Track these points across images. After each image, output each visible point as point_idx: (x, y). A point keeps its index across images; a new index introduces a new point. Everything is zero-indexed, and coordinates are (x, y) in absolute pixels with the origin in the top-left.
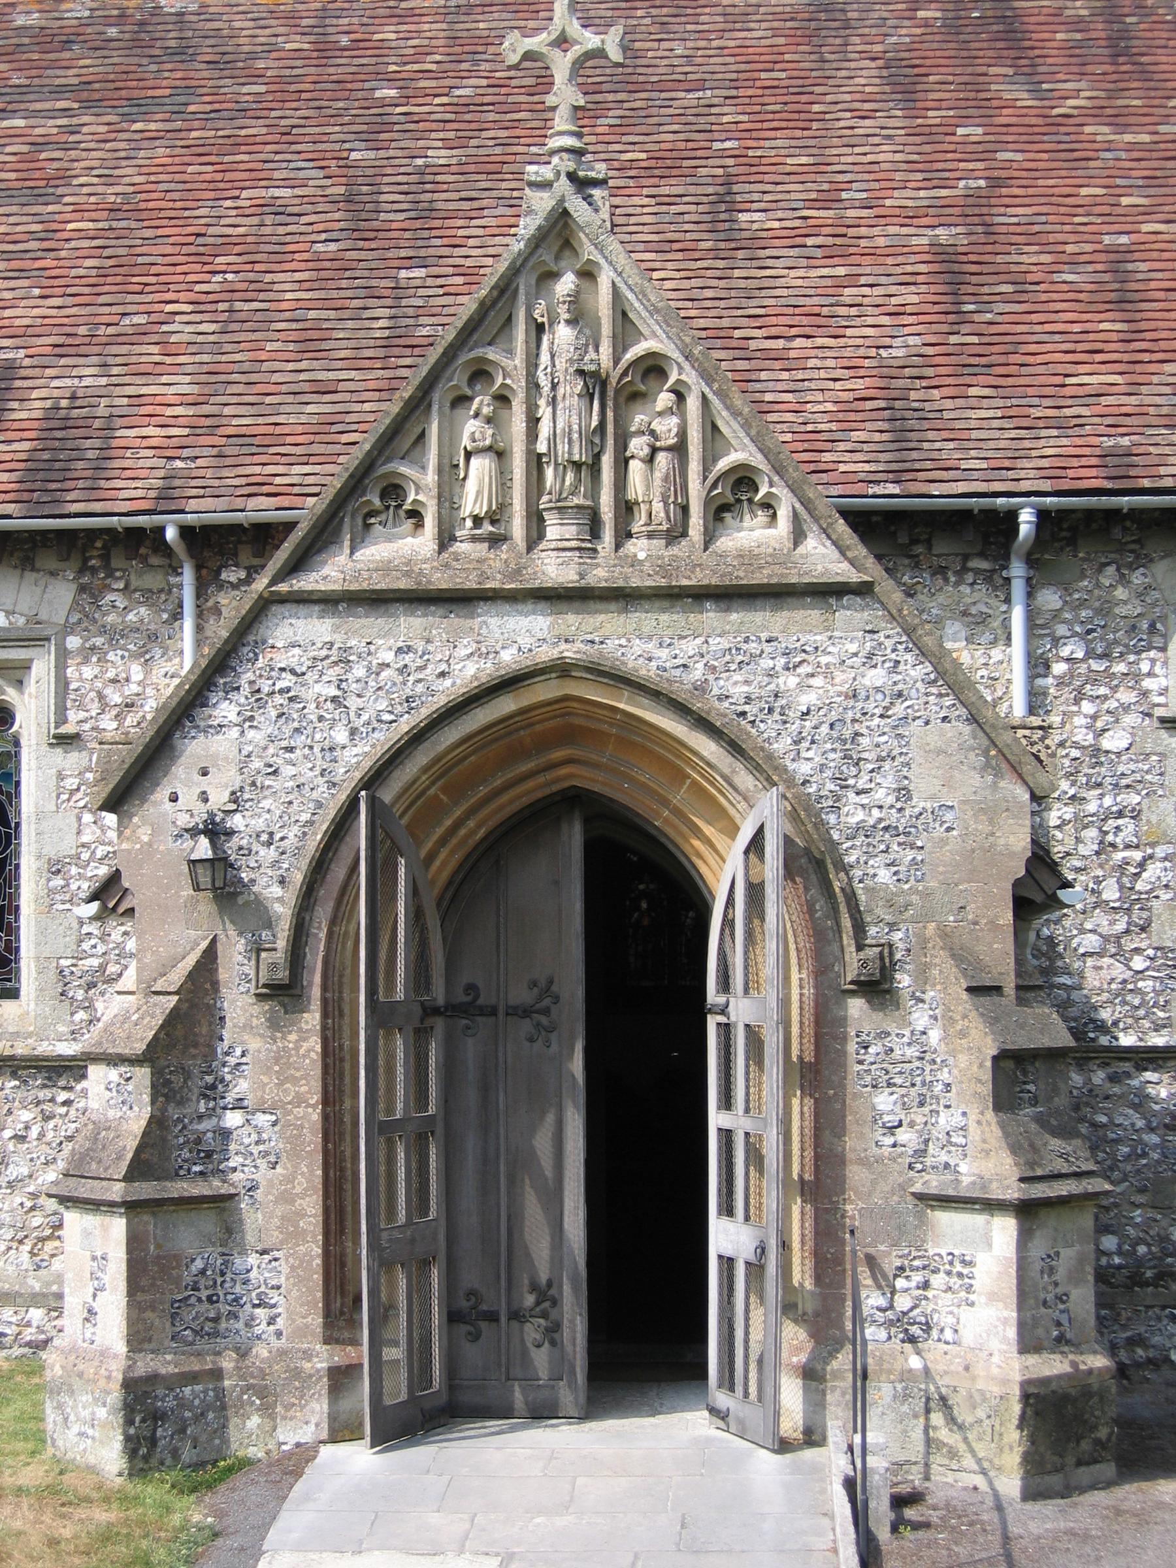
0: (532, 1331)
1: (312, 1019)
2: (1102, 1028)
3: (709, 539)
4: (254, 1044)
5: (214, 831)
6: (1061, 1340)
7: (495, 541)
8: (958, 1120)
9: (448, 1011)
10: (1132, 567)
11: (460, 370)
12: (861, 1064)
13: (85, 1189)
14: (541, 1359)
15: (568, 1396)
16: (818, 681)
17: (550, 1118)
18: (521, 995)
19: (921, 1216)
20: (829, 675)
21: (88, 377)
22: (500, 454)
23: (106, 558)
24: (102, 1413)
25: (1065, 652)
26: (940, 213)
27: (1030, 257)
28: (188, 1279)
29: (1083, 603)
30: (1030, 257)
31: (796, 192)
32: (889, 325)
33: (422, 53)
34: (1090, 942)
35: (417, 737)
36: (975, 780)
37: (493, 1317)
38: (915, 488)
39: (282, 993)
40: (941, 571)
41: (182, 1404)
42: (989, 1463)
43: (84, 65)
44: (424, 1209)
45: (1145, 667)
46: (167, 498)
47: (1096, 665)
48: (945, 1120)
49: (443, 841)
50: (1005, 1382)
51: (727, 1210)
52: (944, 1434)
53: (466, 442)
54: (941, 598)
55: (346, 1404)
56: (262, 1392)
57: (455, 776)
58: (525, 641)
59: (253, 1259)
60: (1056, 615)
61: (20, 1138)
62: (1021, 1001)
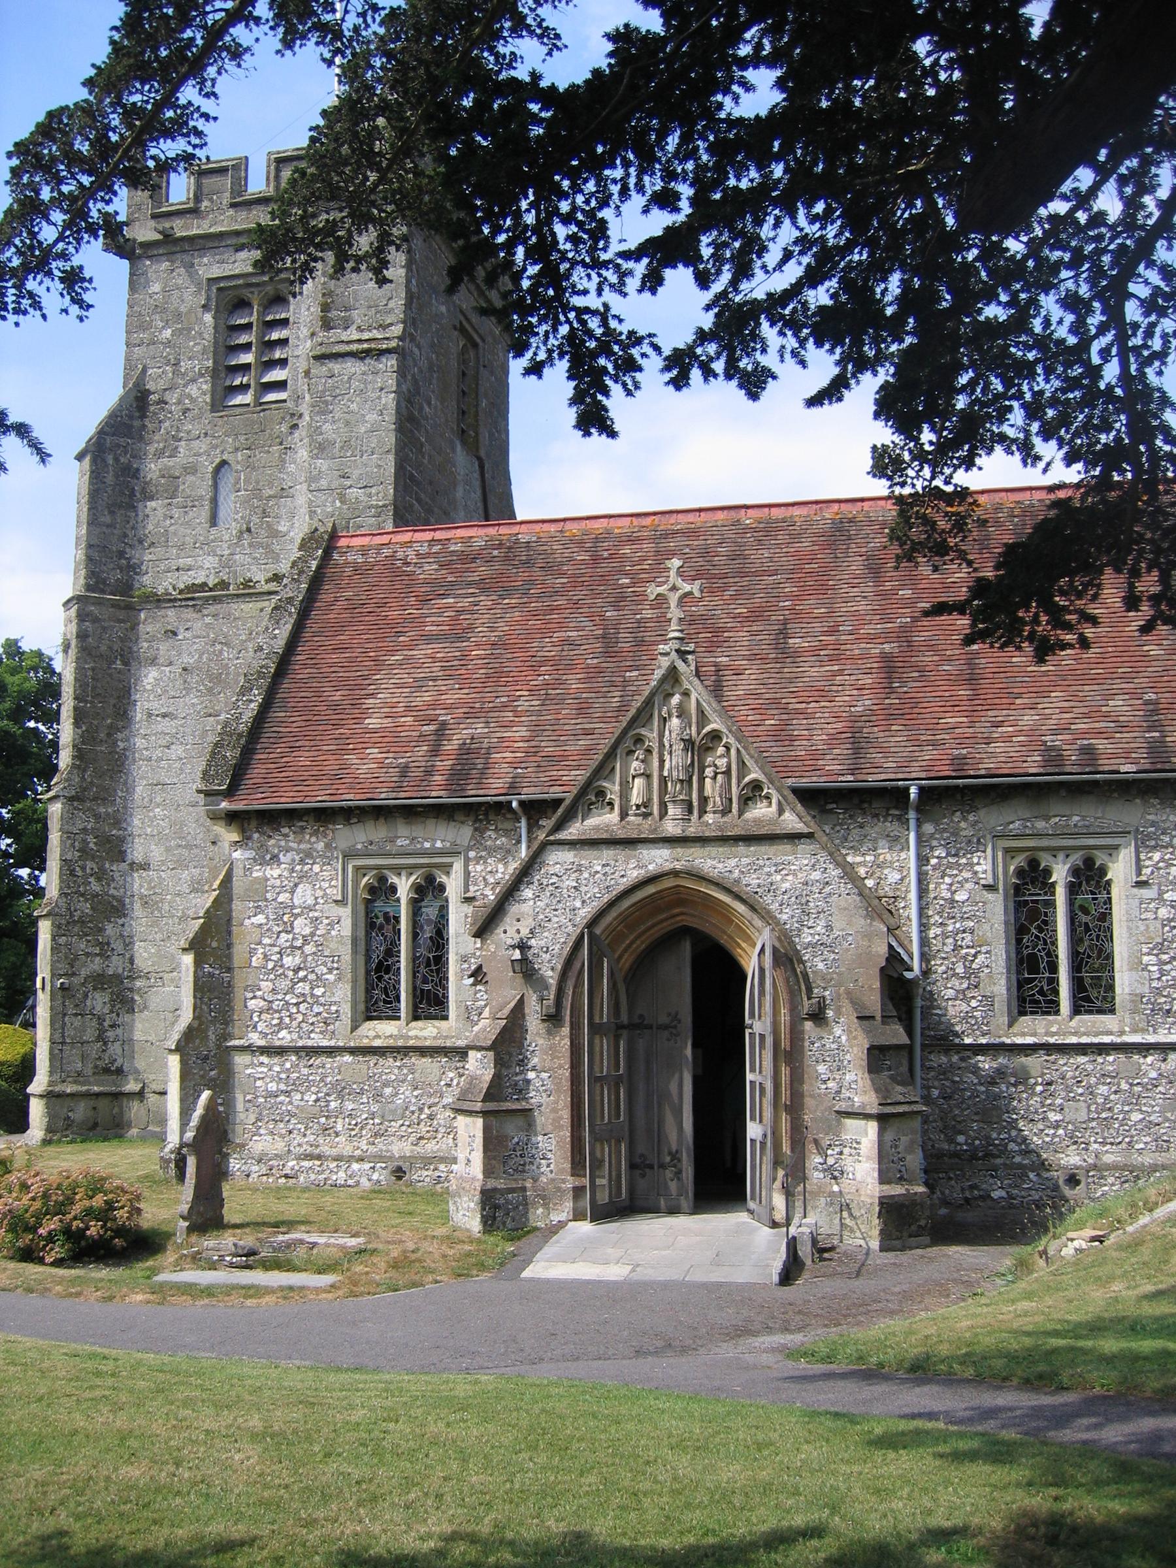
0: (669, 1174)
1: (566, 1030)
2: (956, 1035)
3: (741, 813)
4: (541, 1041)
5: (523, 946)
6: (901, 1178)
7: (646, 816)
8: (853, 1078)
9: (629, 1026)
10: (969, 812)
11: (629, 740)
12: (812, 1050)
13: (466, 1106)
14: (673, 1186)
15: (685, 1204)
16: (790, 878)
17: (677, 1076)
18: (663, 1019)
19: (839, 1123)
20: (795, 875)
21: (480, 729)
22: (648, 777)
23: (486, 814)
24: (472, 1205)
25: (936, 853)
26: (886, 636)
27: (928, 658)
28: (510, 1145)
29: (945, 830)
30: (928, 658)
31: (817, 627)
32: (856, 693)
33: (643, 560)
34: (950, 993)
35: (611, 904)
36: (862, 922)
37: (651, 1167)
38: (860, 777)
39: (553, 1019)
40: (876, 816)
41: (508, 1202)
42: (866, 1234)
43: (482, 570)
44: (618, 1116)
45: (975, 860)
46: (513, 788)
47: (951, 860)
48: (849, 1077)
49: (625, 950)
50: (872, 1197)
51: (753, 1118)
52: (848, 1221)
53: (632, 772)
54: (876, 829)
55: (580, 1204)
56: (544, 1198)
57: (630, 921)
58: (660, 861)
59: (540, 1138)
60: (932, 836)
61: (449, 1085)
62: (883, 1023)
